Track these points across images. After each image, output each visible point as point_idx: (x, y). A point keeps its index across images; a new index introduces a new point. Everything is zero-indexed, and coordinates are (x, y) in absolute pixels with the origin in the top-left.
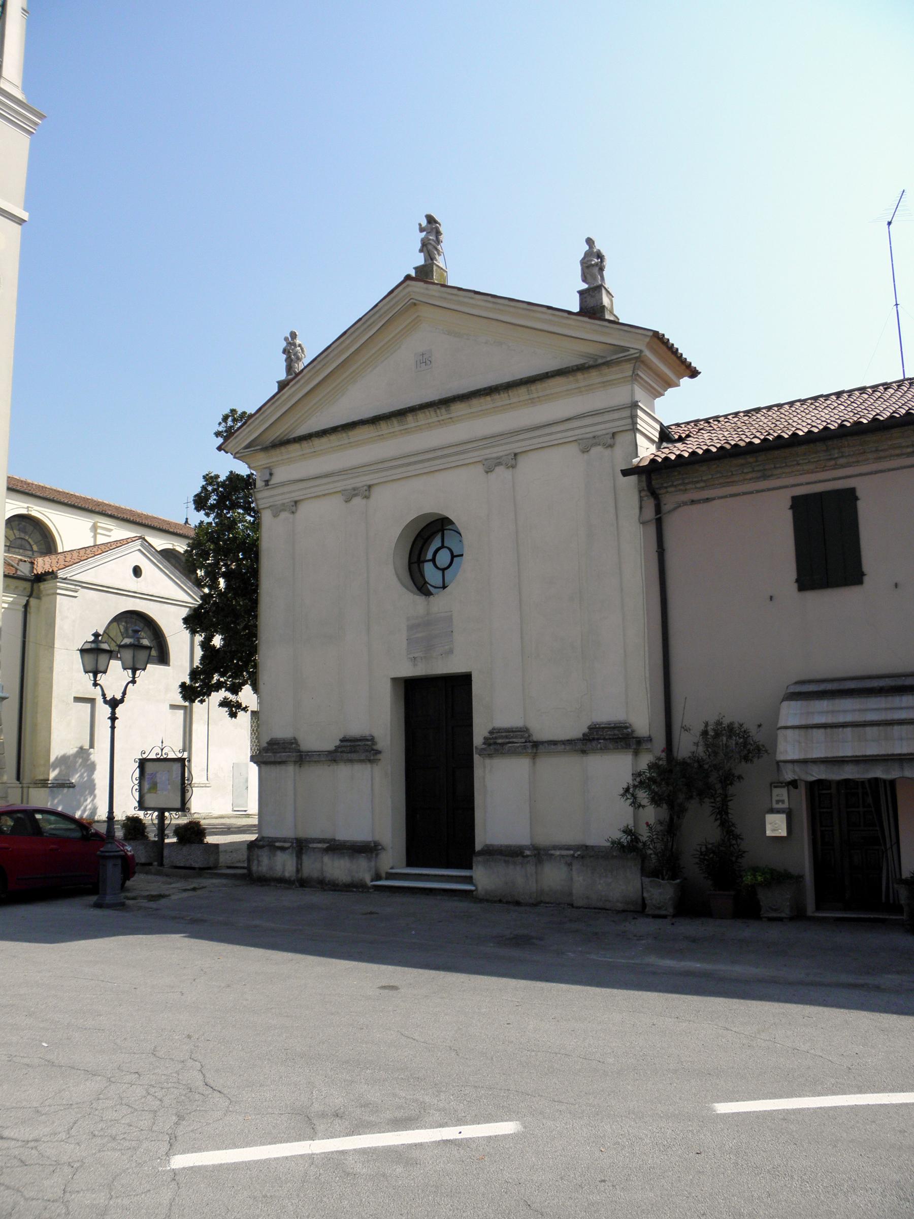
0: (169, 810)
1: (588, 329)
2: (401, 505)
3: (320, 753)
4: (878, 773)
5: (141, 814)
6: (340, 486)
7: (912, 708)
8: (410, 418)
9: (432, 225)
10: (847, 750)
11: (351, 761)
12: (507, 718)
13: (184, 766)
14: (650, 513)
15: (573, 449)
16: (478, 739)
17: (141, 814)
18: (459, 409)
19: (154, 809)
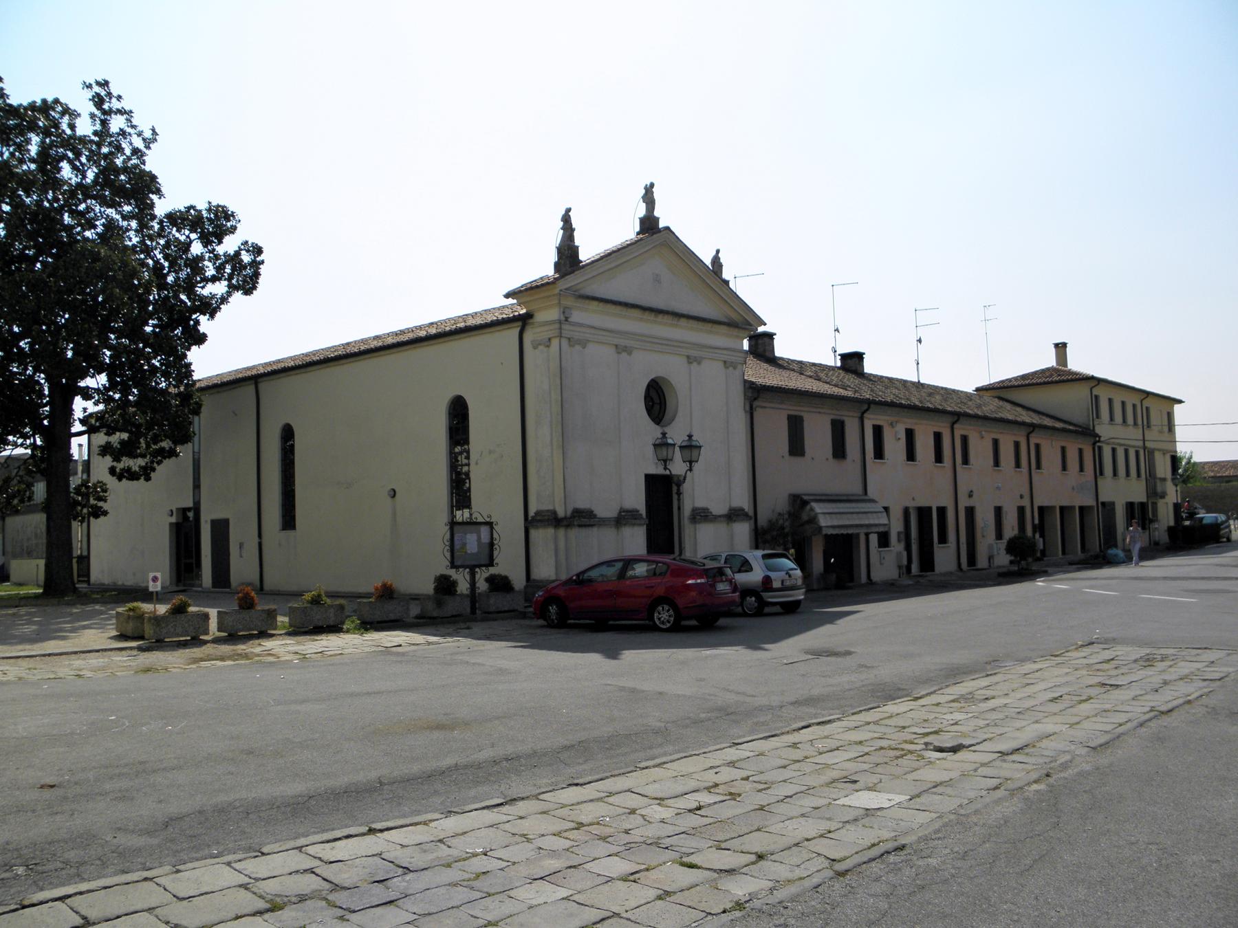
0: (480, 566)
1: (850, 379)
2: (647, 365)
3: (609, 519)
4: (850, 531)
5: (452, 573)
6: (616, 341)
7: (1237, 579)
8: (660, 316)
9: (649, 190)
10: (836, 523)
11: (634, 525)
12: (700, 503)
13: (492, 528)
14: (748, 408)
15: (721, 364)
16: (687, 511)
17: (452, 573)
18: (683, 322)
19: (465, 567)
